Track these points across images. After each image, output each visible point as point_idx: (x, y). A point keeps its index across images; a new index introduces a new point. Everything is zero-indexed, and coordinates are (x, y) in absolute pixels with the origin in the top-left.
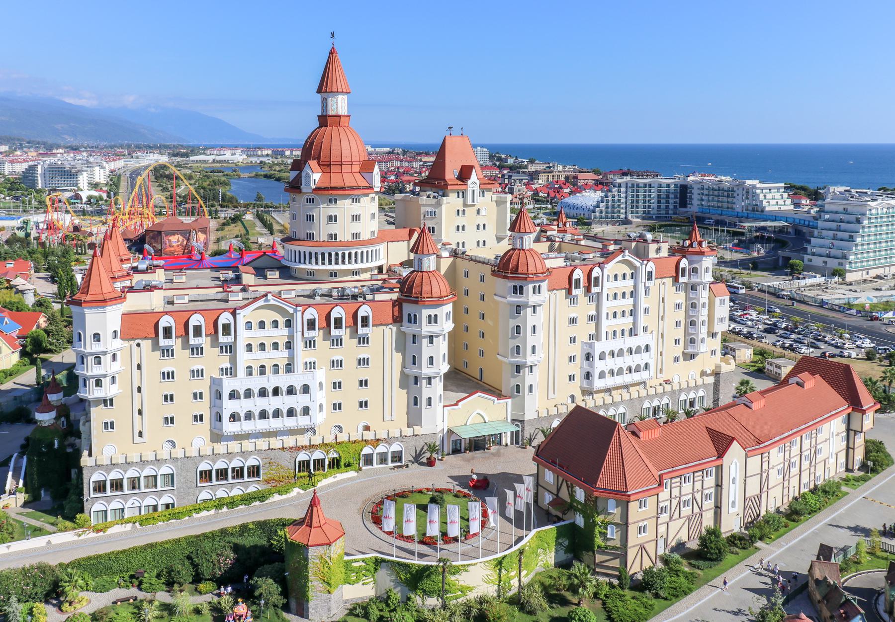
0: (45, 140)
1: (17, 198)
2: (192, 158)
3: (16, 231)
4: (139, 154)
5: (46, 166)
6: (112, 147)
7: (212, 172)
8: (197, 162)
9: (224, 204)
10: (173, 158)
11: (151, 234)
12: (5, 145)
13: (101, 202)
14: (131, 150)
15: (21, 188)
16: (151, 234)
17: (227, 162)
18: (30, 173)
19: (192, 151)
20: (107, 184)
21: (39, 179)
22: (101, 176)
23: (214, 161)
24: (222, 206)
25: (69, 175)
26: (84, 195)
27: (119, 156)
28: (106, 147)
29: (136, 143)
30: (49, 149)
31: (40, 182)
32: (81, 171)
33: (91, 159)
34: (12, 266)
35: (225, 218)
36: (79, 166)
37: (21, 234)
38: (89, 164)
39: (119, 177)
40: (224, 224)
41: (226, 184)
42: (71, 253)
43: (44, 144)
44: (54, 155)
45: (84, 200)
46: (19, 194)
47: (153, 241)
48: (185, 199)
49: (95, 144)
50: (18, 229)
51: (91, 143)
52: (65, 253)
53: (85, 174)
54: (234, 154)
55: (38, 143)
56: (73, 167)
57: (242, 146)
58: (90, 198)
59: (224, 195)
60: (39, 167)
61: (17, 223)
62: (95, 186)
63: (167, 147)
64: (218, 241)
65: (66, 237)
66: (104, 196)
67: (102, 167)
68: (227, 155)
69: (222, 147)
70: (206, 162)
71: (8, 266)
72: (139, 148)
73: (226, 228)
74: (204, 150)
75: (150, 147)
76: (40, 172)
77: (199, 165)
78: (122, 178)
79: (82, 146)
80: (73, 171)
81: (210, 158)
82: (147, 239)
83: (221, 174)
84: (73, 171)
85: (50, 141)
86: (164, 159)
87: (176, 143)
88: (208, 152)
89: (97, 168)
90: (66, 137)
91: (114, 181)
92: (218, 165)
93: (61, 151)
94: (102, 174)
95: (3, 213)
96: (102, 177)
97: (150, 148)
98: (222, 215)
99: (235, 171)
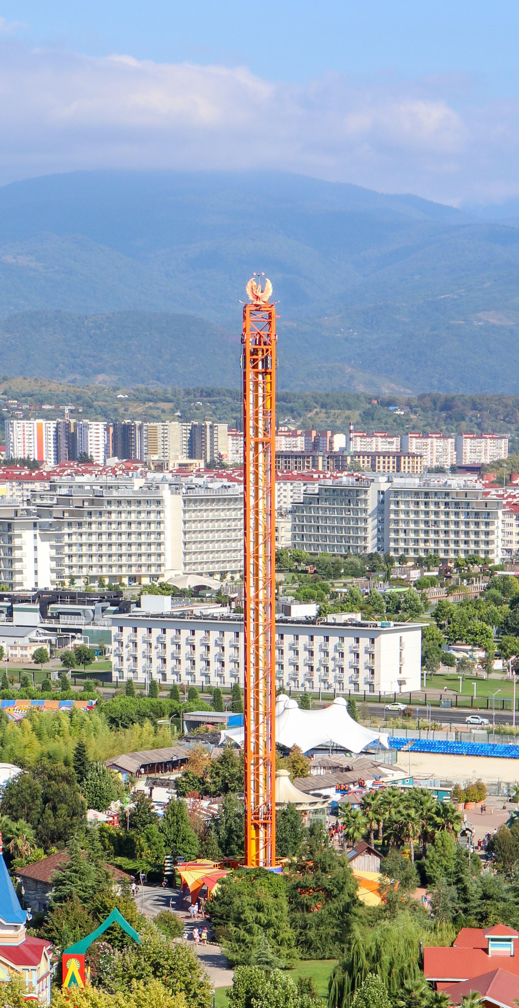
12: (495, 433)
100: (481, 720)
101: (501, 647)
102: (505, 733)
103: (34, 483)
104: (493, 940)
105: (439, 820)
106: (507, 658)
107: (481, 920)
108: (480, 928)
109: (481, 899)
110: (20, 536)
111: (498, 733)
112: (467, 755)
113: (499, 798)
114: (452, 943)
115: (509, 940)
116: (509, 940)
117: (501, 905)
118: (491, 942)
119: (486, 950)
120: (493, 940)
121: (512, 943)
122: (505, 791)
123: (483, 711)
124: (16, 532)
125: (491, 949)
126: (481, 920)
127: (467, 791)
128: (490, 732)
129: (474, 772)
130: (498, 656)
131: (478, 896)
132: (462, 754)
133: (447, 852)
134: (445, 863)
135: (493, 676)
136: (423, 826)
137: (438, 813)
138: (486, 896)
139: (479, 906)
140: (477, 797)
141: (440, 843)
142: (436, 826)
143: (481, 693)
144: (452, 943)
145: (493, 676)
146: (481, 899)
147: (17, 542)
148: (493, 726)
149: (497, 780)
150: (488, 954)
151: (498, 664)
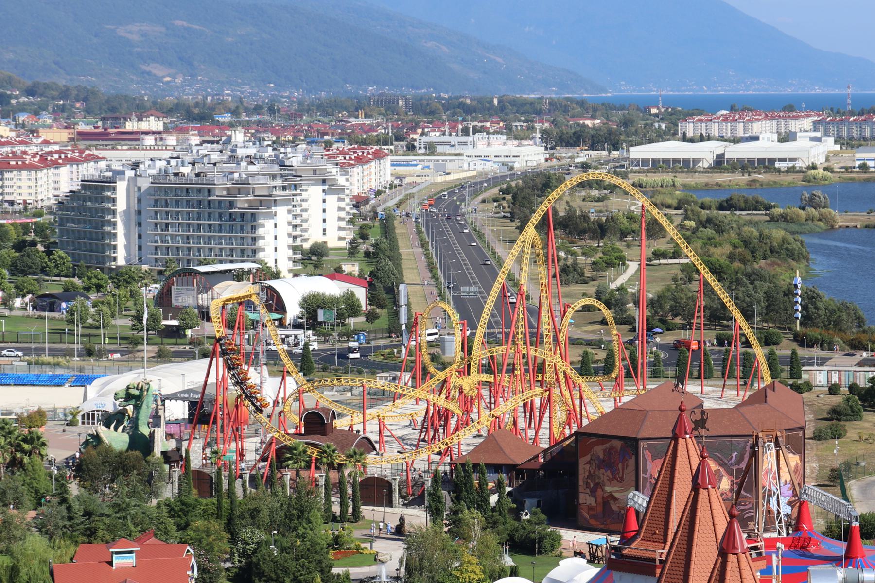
0: (86, 80)
1: (47, 303)
2: (639, 152)
3: (102, 430)
4: (434, 136)
5: (145, 184)
6: (327, 108)
7: (728, 205)
8: (656, 165)
9: (815, 333)
10: (564, 153)
11: (599, 450)
13: (352, 321)
14: (407, 119)
15: (54, 258)
16: (599, 450)
17: (767, 165)
18: (87, 207)
19: (626, 123)
20: (352, 251)
21: (120, 230)
22: (325, 220)
23: (720, 163)
24: (802, 341)
25: (230, 218)
26: (294, 291)
27: (365, 147)
28: (302, 109)
29: (411, 93)
30: (108, 118)
31: (121, 241)
32: (267, 202)
33: (296, 159)
34: (129, 561)
35: (833, 390)
36: (261, 184)
37: (116, 439)
38: (292, 179)
39: (387, 228)
40: (836, 414)
41: (791, 254)
42: (317, 515)
43: (87, 96)
44: (135, 137)
45: (293, 310)
46: (53, 286)
47: (604, 475)
48: (668, 310)
49: (263, 98)
50: (111, 419)
51: (253, 92)
52: (296, 514)
53: (282, 213)
54: (786, 137)
55: (65, 94)
56: (241, 187)
57: (813, 105)
58: (312, 305)
59: (811, 298)
60: (121, 187)
61: (104, 392)
62: (313, 259)
63: (530, 110)
64: (836, 479)
65: (280, 456)
66: (361, 294)
67: (331, 187)
68: (765, 142)
69: (740, 108)
70: (687, 165)
71: (117, 561)
72: (426, 111)
73: (852, 429)
74: (670, 123)
75: (468, 111)
76: (121, 205)
77: (668, 178)
78: (399, 230)
79: (221, 106)
80: (242, 202)
81: (705, 153)
82: (584, 468)
83: (760, 216)
84: (242, 202)
85: (105, 86)
86: (531, 155)
87: (553, 94)
88: (690, 129)
89: (314, 193)
90: (157, 70)
91: (375, 243)
92: (739, 178)
93: (153, 123)
94: (333, 215)
95: (15, 362)
96: (333, 225)
97: (469, 113)
98: (819, 376)
99: (812, 202)
100: (16, 353)
101: (17, 287)
102: (43, 364)
103: (12, 172)
104: (117, 553)
105: (26, 447)
106: (24, 296)
107: (90, 536)
108: (90, 542)
109: (84, 516)
110: (263, 226)
111: (36, 363)
112: (15, 385)
113: (55, 422)
114: (72, 559)
115: (131, 552)
116: (131, 552)
117: (107, 520)
118: (115, 556)
119: (111, 563)
120: (117, 553)
121: (134, 555)
122: (61, 416)
123: (13, 345)
124: (261, 221)
125: (115, 562)
126: (90, 536)
127: (30, 417)
128: (30, 363)
129: (28, 400)
130: (17, 296)
131: (81, 513)
132: (9, 385)
133: (37, 476)
134: (35, 485)
135: (14, 313)
136: (12, 453)
137: (25, 440)
138: (88, 514)
139: (82, 523)
140: (39, 423)
141: (30, 468)
142: (24, 452)
143: (10, 329)
144: (72, 559)
145: (14, 313)
146: (84, 516)
147: (260, 231)
148: (32, 358)
149: (52, 406)
150: (112, 566)
151: (18, 302)
